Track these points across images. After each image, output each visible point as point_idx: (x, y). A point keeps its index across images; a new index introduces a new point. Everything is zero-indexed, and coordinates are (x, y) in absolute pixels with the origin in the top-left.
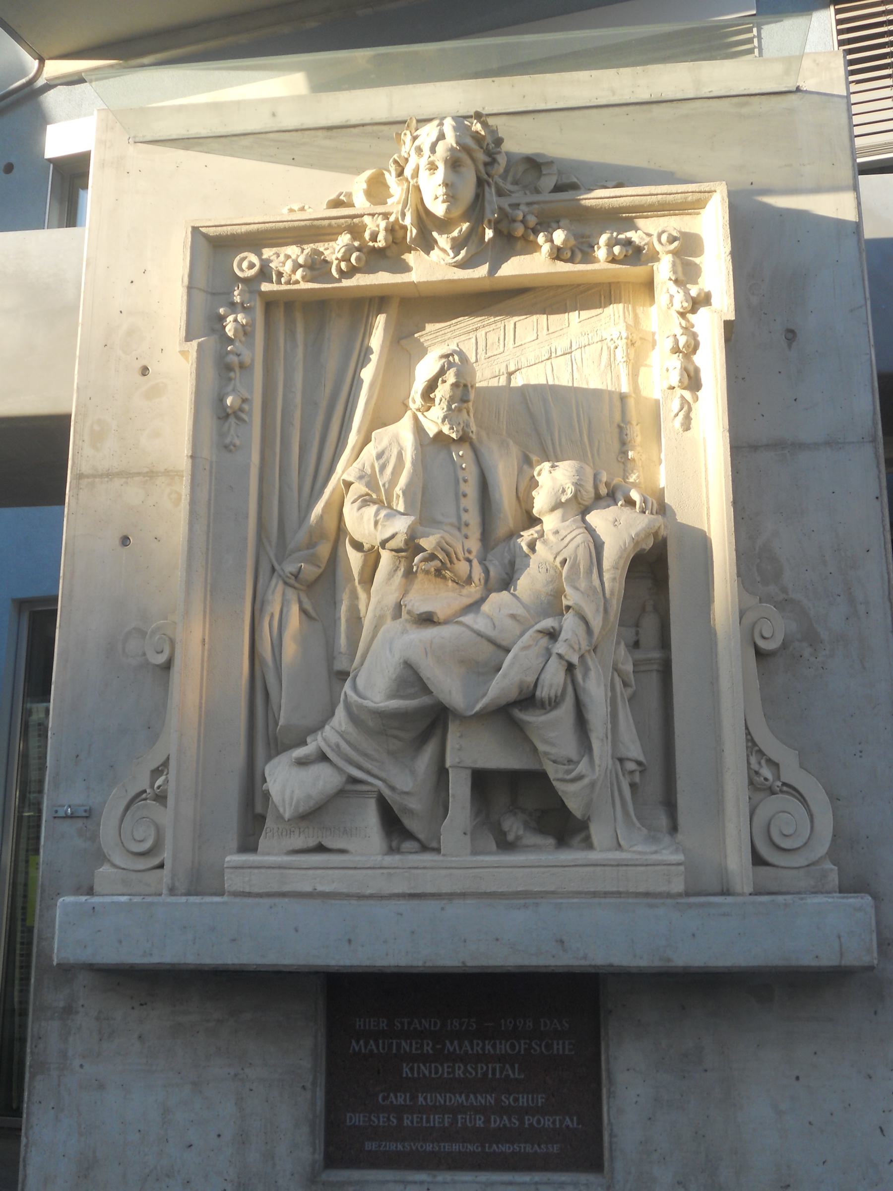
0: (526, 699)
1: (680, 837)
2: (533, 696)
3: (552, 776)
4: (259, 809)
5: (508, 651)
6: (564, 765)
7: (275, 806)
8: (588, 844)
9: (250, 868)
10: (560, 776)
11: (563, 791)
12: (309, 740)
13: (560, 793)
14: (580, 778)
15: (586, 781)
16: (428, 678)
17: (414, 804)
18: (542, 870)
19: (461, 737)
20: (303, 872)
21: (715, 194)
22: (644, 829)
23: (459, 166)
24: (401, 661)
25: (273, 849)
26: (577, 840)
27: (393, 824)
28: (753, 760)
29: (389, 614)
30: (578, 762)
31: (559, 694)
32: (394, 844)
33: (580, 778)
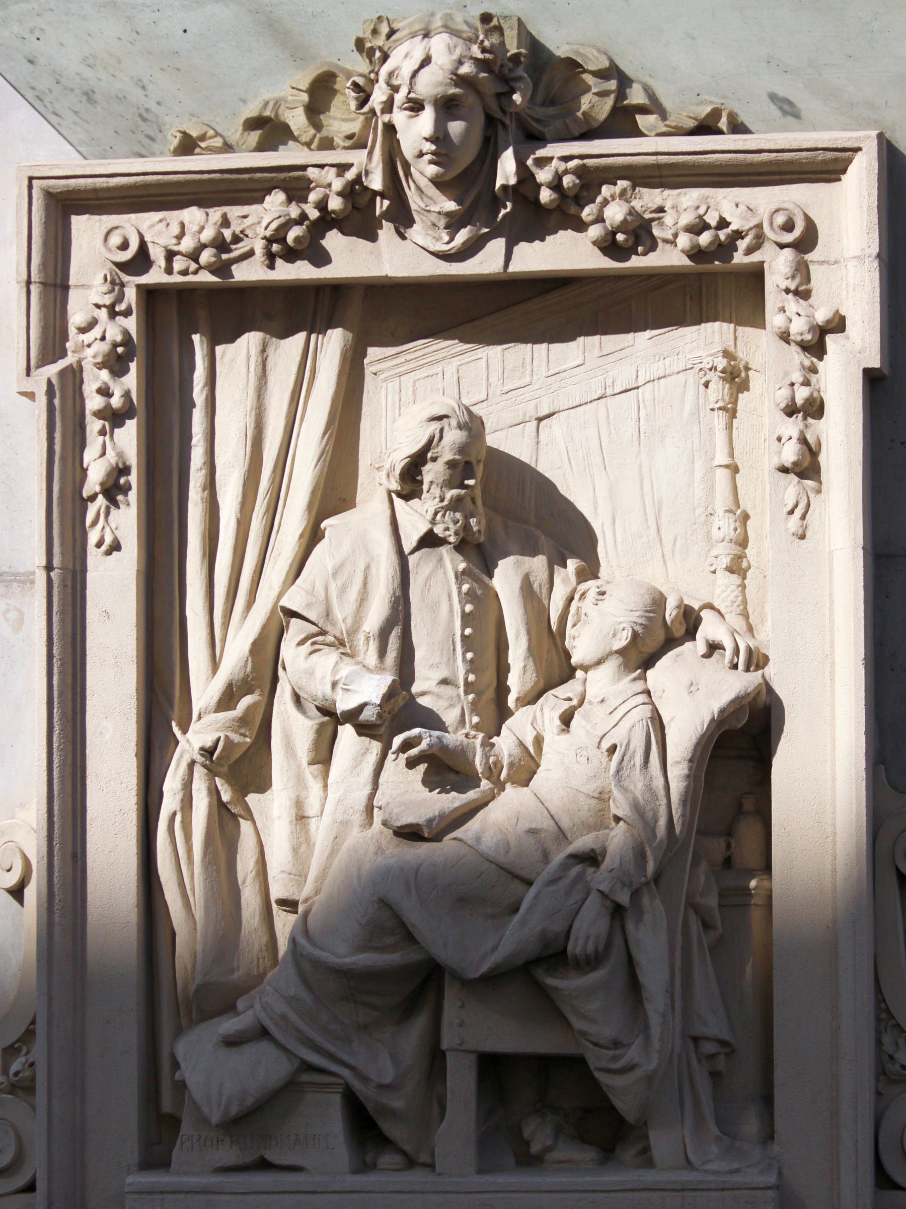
0: (555, 955)
1: (776, 1148)
2: (564, 951)
3: (592, 1063)
4: (167, 1106)
5: (530, 883)
6: (608, 1049)
7: (195, 1103)
8: (646, 1158)
9: (162, 1192)
10: (603, 1064)
11: (607, 1086)
12: (241, 1004)
13: (604, 1089)
14: (630, 1068)
15: (638, 1073)
16: (414, 926)
17: (397, 1102)
18: (578, 1195)
19: (462, 1007)
20: (240, 1197)
21: (860, 153)
22: (725, 1138)
23: (457, 105)
24: (375, 898)
25: (195, 1162)
26: (628, 1153)
27: (365, 1127)
28: (887, 1039)
29: (358, 818)
30: (629, 1045)
31: (601, 949)
32: (369, 1158)
33: (630, 1068)
